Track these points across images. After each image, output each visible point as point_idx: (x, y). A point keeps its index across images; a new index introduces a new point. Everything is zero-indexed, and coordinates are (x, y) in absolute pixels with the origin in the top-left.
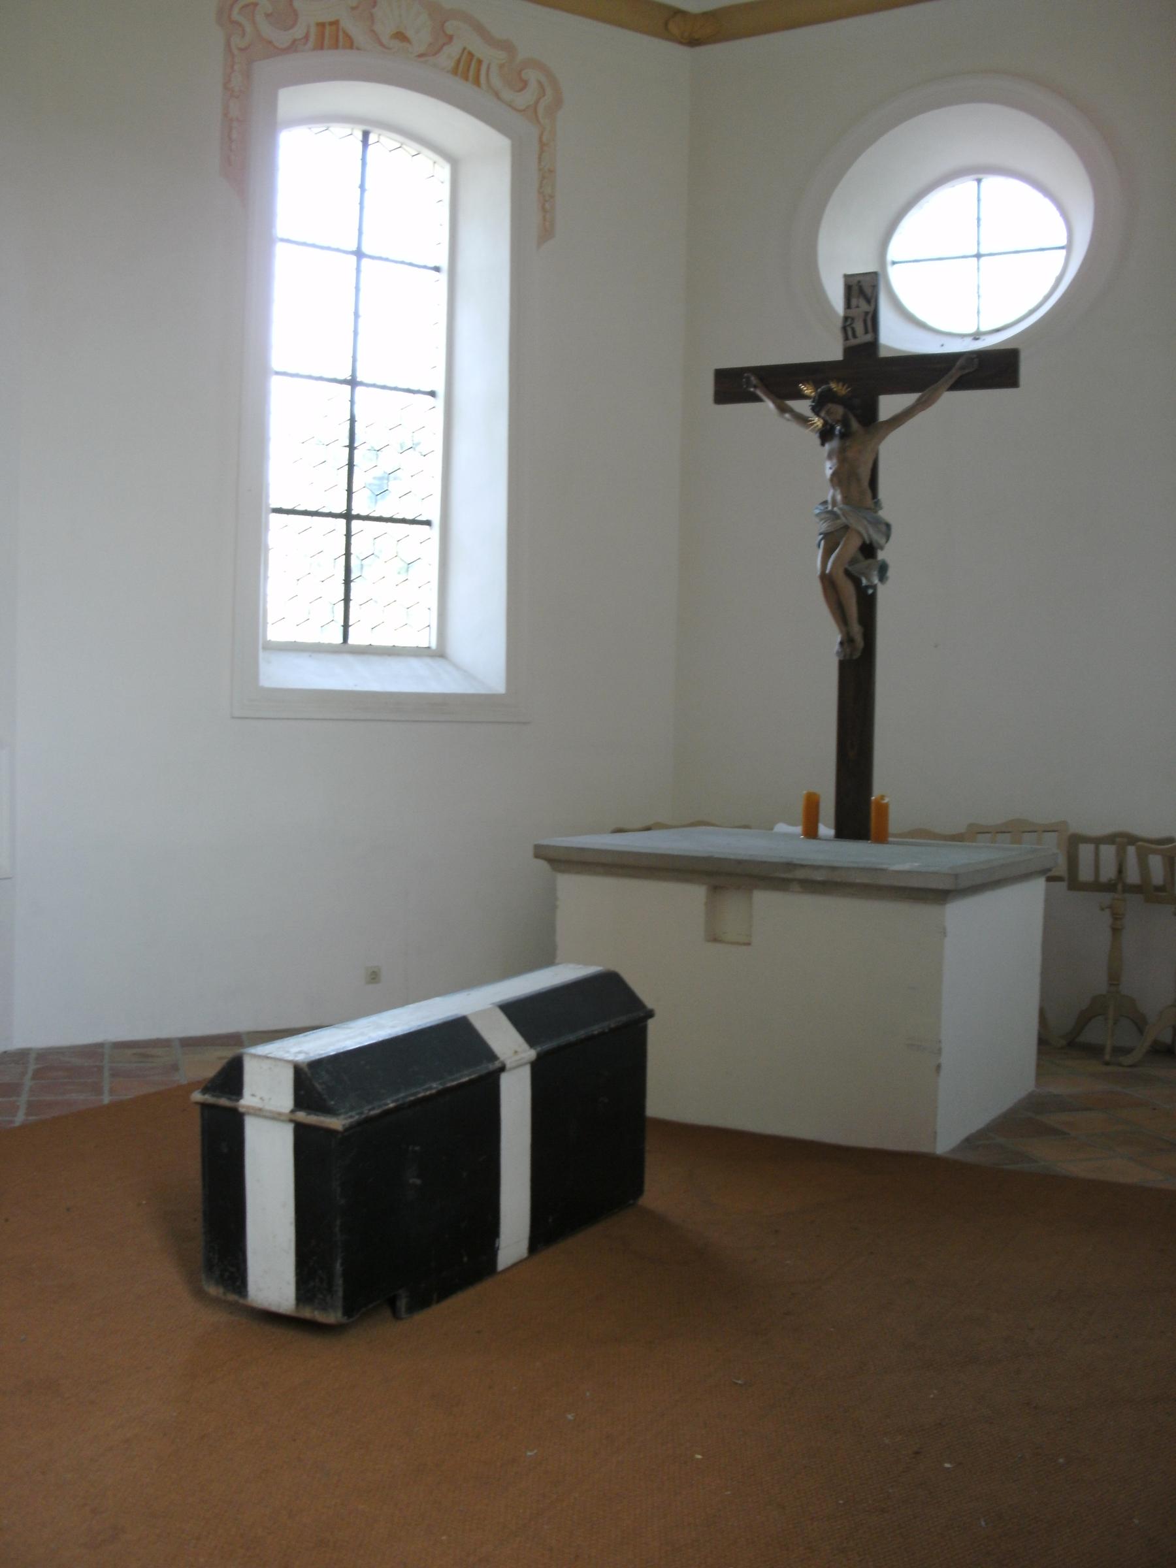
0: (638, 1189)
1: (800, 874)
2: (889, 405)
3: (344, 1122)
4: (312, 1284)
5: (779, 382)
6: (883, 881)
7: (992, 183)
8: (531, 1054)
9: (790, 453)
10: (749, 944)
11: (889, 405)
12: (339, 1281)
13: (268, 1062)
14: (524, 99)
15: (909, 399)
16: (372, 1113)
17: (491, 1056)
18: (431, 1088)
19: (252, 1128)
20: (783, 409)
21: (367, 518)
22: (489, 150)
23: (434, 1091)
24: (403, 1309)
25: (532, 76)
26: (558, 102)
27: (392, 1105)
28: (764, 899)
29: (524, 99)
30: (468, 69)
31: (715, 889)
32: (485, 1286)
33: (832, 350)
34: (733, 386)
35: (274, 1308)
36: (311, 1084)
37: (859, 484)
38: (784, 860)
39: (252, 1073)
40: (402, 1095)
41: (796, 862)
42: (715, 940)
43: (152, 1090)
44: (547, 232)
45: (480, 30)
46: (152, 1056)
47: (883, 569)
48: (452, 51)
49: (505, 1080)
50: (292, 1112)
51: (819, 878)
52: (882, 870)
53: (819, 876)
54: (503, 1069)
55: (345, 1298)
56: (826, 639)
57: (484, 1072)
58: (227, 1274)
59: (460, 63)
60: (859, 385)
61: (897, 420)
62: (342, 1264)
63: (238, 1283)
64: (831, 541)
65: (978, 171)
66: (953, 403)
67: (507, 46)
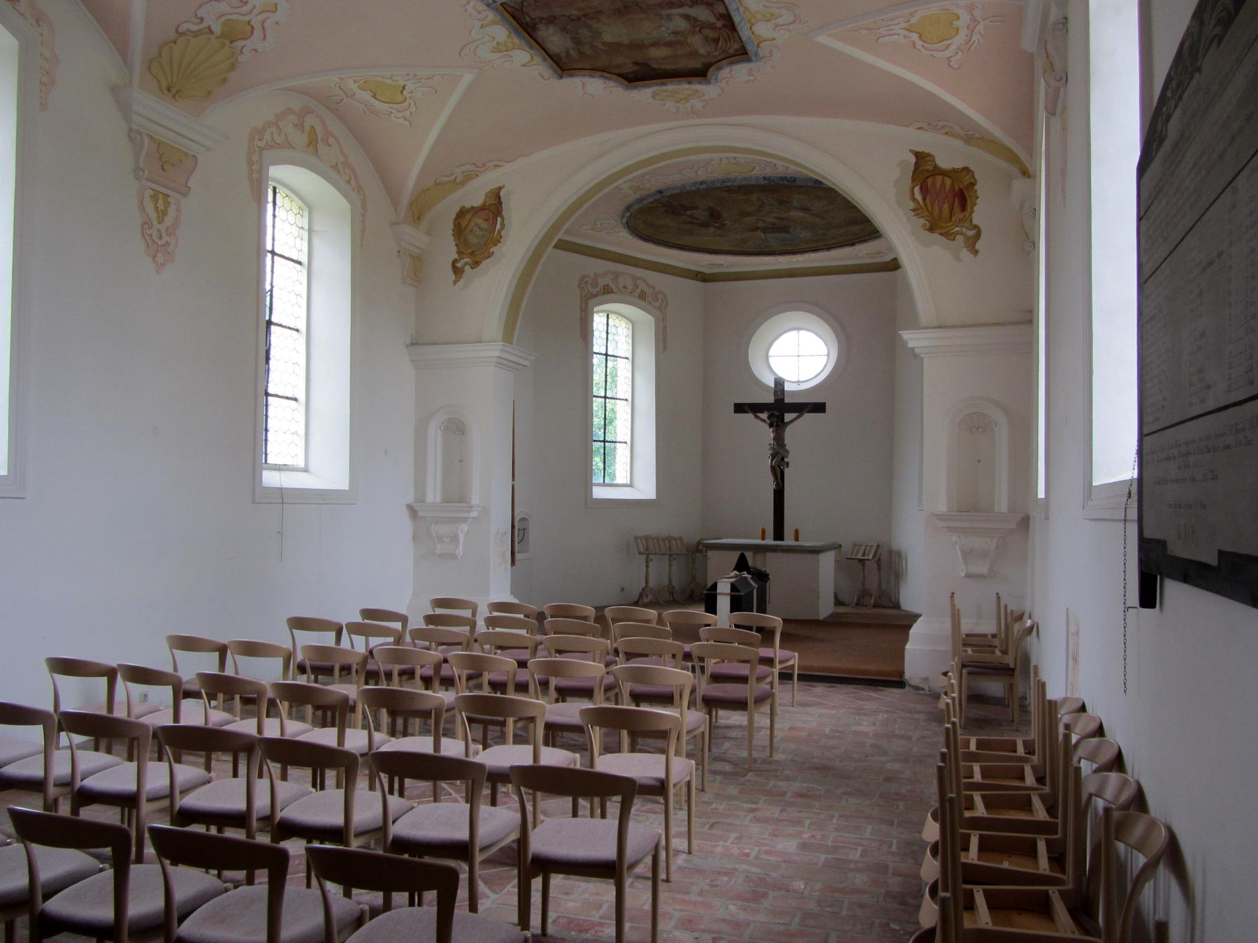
2: (788, 417)
5: (755, 408)
7: (802, 332)
9: (759, 431)
11: (788, 417)
14: (658, 304)
15: (795, 415)
19: (719, 598)
20: (757, 417)
21: (277, 396)
22: (645, 319)
25: (660, 296)
26: (666, 305)
29: (658, 304)
30: (643, 296)
33: (771, 400)
34: (740, 408)
37: (779, 439)
44: (665, 348)
45: (647, 284)
47: (788, 464)
48: (638, 290)
56: (770, 485)
59: (642, 297)
60: (779, 409)
61: (791, 422)
64: (773, 456)
65: (798, 329)
66: (808, 416)
67: (653, 287)
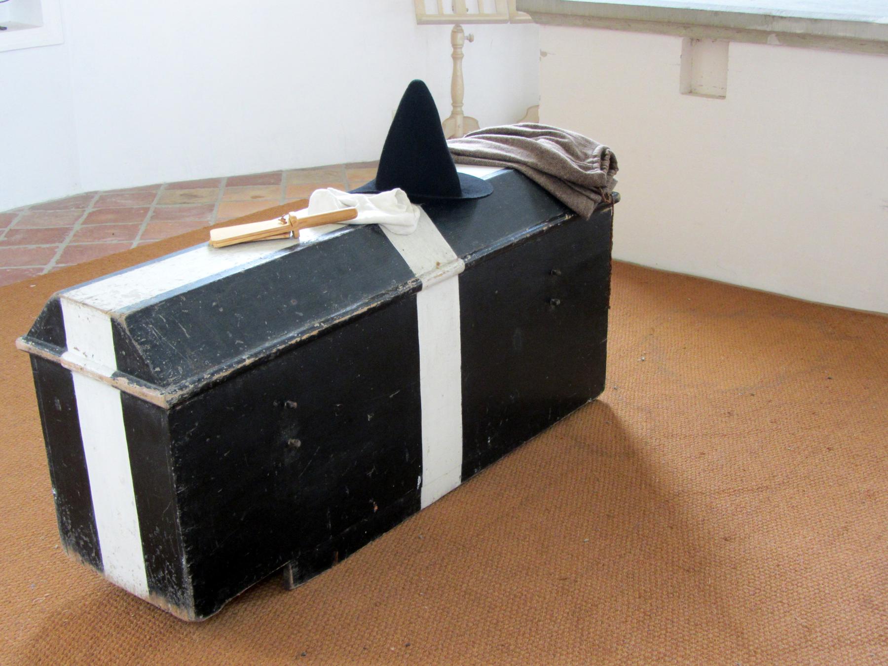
0: (595, 378)
1: (778, 27)
3: (169, 397)
4: (161, 574)
6: (867, 35)
8: (460, 265)
10: (723, 97)
12: (188, 579)
13: (86, 309)
16: (216, 377)
17: (405, 272)
18: (313, 328)
23: (315, 333)
24: (292, 581)
27: (248, 362)
28: (740, 52)
31: (694, 41)
32: (408, 524)
35: (130, 589)
36: (139, 340)
38: (761, 12)
39: (71, 317)
40: (267, 345)
41: (774, 14)
42: (691, 92)
43: (189, 230)
46: (196, 196)
49: (422, 300)
50: (115, 375)
51: (798, 31)
52: (867, 23)
53: (799, 29)
54: (419, 288)
55: (196, 596)
57: (388, 298)
58: (82, 543)
62: (188, 561)
63: (93, 555)
